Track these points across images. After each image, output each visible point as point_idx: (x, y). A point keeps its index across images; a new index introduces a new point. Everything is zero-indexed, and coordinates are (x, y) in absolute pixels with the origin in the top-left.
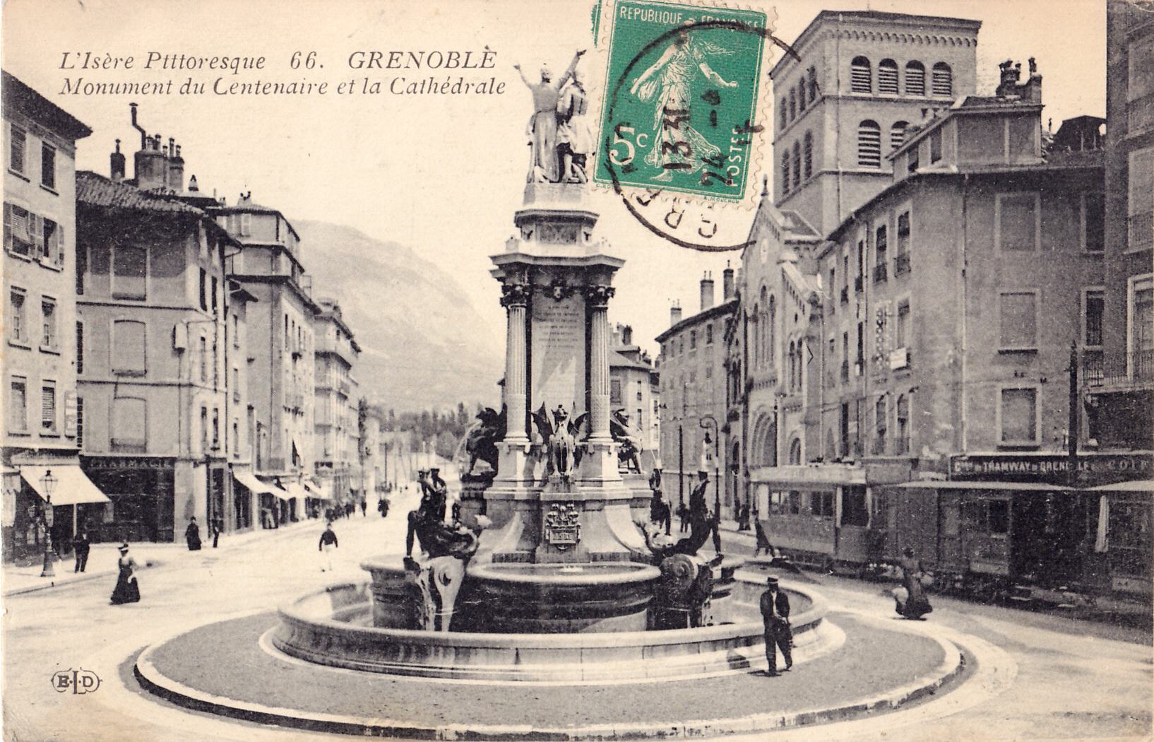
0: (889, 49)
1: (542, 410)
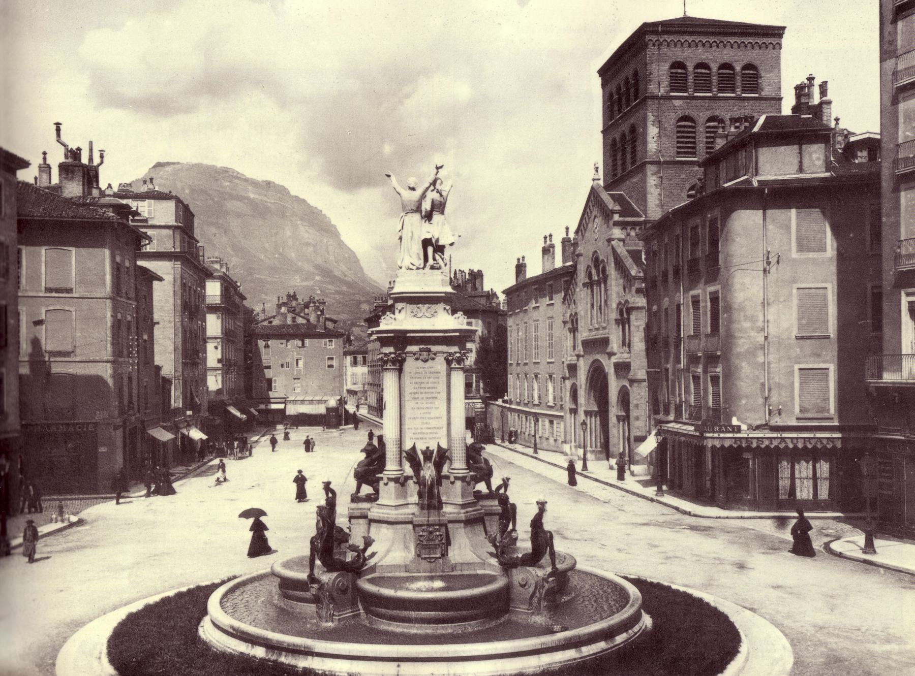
0: (702, 54)
1: (414, 448)
